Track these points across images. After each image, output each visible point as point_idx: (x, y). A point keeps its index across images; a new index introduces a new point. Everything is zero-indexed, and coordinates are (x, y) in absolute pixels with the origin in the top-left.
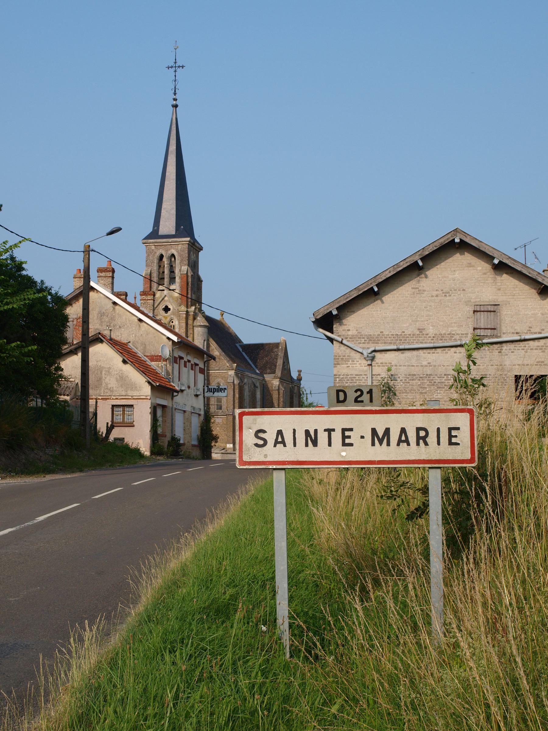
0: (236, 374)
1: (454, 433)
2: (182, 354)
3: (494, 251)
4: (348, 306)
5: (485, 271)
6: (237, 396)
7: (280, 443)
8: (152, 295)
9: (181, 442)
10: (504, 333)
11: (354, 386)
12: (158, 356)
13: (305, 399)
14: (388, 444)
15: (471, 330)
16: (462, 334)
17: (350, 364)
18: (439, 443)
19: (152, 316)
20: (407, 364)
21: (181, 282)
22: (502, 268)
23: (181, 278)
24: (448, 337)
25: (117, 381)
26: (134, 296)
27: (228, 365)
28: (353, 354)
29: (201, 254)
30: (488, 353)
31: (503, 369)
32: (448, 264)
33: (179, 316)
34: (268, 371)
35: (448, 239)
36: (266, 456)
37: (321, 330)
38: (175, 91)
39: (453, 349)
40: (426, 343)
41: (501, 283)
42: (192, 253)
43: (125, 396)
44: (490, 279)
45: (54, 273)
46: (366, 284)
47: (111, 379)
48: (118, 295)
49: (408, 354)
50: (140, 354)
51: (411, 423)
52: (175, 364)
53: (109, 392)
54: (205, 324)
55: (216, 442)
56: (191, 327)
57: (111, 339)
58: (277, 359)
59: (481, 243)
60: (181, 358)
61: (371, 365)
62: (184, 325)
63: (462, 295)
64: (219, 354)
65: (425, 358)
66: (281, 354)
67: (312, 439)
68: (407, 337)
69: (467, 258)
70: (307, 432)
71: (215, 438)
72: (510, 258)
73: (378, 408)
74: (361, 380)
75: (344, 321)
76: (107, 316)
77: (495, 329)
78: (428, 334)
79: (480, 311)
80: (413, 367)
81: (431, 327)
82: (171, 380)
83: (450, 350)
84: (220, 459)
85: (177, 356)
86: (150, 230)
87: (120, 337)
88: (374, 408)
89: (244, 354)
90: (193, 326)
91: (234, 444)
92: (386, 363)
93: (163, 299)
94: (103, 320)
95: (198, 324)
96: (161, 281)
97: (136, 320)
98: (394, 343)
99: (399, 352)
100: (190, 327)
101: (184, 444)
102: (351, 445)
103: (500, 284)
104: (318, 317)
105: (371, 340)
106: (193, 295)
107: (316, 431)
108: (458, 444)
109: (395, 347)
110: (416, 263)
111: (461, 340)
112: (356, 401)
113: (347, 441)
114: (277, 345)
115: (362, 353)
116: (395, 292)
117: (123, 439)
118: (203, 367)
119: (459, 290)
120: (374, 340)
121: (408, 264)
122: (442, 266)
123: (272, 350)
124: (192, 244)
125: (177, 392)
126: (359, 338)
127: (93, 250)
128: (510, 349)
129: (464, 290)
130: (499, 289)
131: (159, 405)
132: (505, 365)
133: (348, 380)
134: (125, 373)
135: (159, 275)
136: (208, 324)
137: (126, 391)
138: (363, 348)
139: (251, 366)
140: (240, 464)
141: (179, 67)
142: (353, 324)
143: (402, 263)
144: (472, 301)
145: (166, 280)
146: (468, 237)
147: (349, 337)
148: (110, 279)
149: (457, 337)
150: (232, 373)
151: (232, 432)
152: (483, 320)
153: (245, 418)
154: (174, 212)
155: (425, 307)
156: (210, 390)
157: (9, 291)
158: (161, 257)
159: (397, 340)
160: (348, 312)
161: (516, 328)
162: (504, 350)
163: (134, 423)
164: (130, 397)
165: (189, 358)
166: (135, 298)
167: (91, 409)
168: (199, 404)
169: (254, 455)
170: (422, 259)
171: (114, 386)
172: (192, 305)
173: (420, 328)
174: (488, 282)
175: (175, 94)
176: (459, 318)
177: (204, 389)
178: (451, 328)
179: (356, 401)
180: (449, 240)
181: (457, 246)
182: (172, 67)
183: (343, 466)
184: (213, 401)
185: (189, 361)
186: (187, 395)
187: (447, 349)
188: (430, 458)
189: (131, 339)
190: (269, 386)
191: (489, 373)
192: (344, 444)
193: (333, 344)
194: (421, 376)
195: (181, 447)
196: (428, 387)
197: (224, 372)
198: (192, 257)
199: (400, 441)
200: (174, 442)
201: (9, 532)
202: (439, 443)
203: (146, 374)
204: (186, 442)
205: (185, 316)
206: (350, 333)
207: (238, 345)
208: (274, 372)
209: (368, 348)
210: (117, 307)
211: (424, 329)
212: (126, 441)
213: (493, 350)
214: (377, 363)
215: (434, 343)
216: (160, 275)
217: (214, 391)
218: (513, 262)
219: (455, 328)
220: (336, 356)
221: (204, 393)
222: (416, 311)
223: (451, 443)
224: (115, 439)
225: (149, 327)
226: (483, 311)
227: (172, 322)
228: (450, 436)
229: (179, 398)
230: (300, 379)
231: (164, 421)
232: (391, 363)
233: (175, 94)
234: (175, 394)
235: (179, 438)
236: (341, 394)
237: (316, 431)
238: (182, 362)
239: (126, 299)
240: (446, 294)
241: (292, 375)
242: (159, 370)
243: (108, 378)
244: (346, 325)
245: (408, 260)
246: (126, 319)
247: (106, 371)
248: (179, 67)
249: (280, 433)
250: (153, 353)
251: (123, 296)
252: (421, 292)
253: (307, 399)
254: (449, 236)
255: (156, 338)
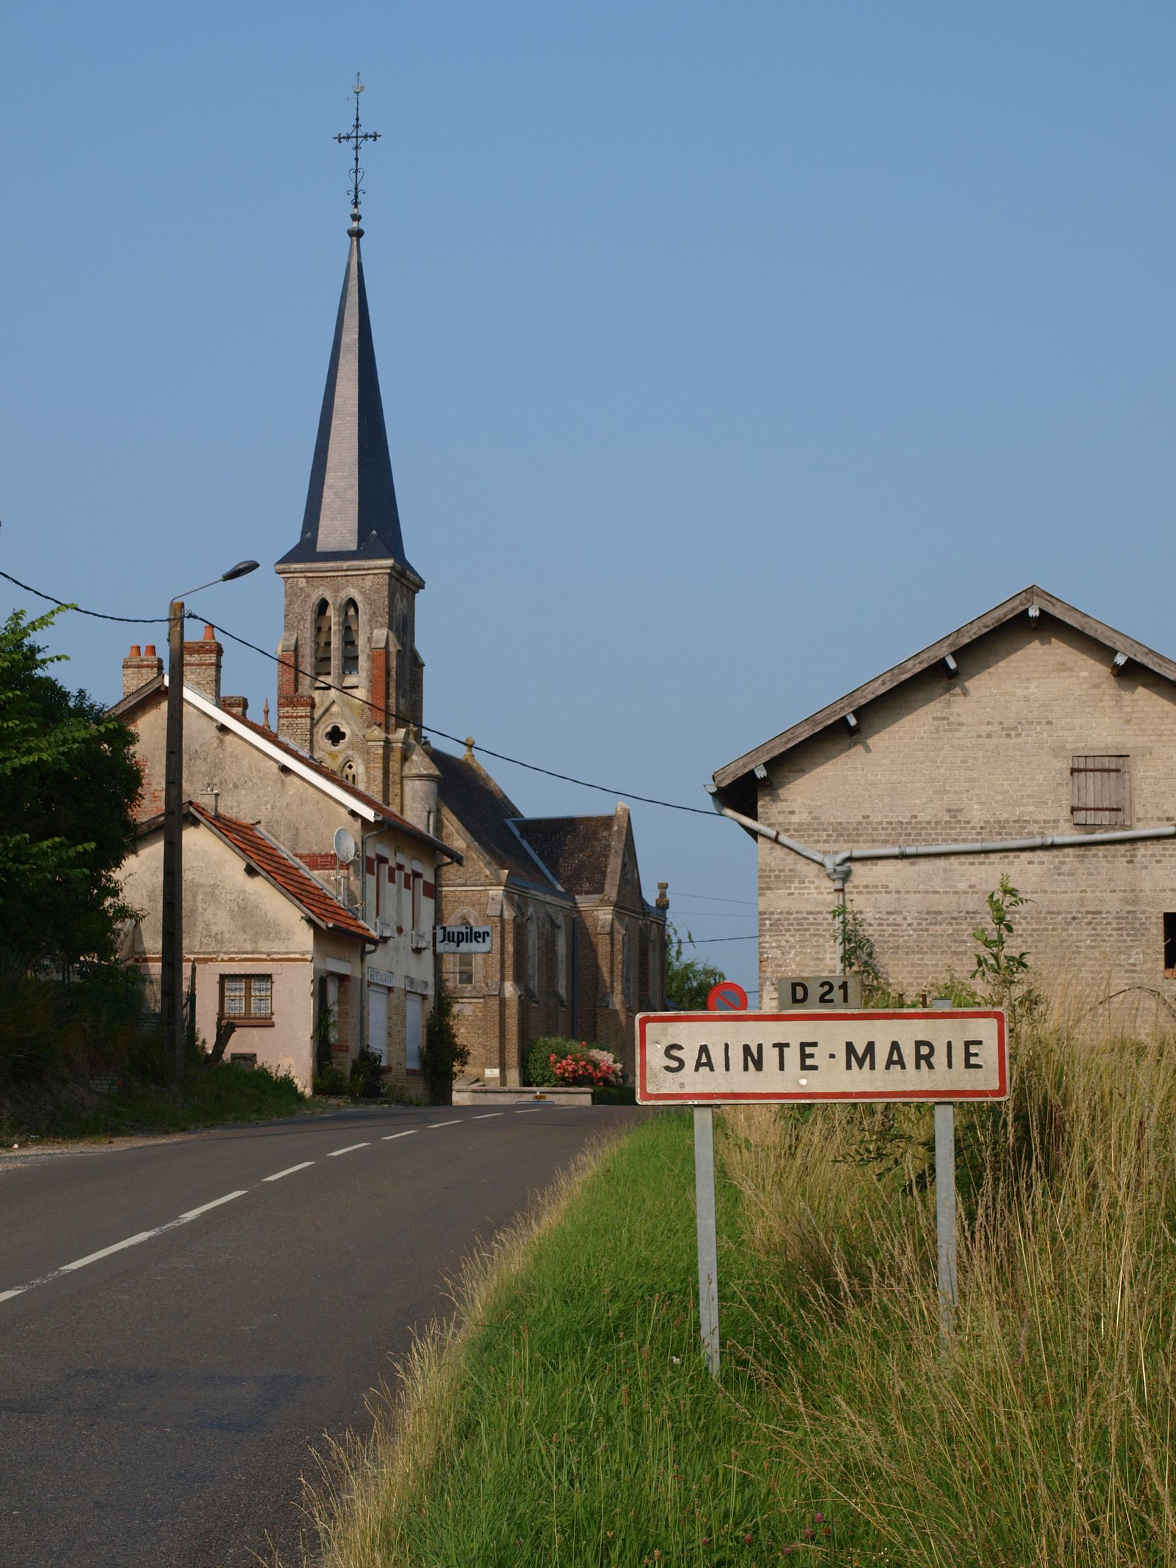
0: (508, 895)
1: (973, 1049)
2: (385, 852)
3: (1117, 636)
4: (792, 758)
5: (1096, 681)
6: (510, 948)
7: (704, 1065)
8: (307, 705)
9: (384, 1063)
10: (1139, 820)
11: (819, 977)
12: (327, 855)
13: (673, 953)
14: (872, 1067)
15: (1066, 813)
16: (1046, 822)
17: (796, 888)
18: (950, 1065)
19: (307, 756)
20: (922, 888)
21: (372, 669)
22: (1133, 673)
23: (372, 659)
24: (1014, 828)
25: (233, 917)
26: (263, 707)
27: (488, 872)
28: (802, 866)
29: (420, 597)
30: (1104, 864)
31: (1136, 902)
32: (1013, 665)
33: (367, 755)
34: (586, 886)
35: (1013, 610)
36: (682, 1085)
37: (729, 812)
38: (356, 197)
39: (1026, 855)
40: (964, 841)
41: (1133, 707)
42: (398, 596)
43: (252, 953)
44: (1107, 698)
45: (91, 668)
46: (830, 710)
47: (219, 912)
48: (224, 704)
49: (924, 865)
50: (285, 852)
51: (908, 1033)
52: (368, 876)
53: (213, 944)
54: (431, 772)
55: (464, 1063)
56: (397, 779)
57: (218, 817)
58: (607, 857)
59: (1087, 620)
60: (382, 860)
61: (842, 890)
62: (379, 774)
63: (1045, 734)
64: (464, 845)
65: (963, 875)
66: (617, 845)
67: (753, 1058)
68: (923, 828)
69: (1059, 650)
70: (747, 1049)
71: (462, 1055)
72: (1151, 651)
73: (856, 1011)
74: (821, 924)
75: (783, 792)
76: (205, 759)
77: (1118, 810)
78: (968, 822)
79: (1086, 770)
80: (936, 896)
81: (976, 807)
82: (360, 915)
83: (1018, 857)
84: (469, 1103)
85: (373, 857)
86: (293, 539)
87: (235, 810)
88: (849, 1012)
89: (524, 843)
90: (402, 778)
91: (503, 1067)
92: (876, 887)
93: (327, 710)
94: (195, 769)
95: (415, 771)
96: (322, 662)
97: (275, 769)
98: (894, 842)
99: (906, 862)
100: (395, 778)
101: (388, 1069)
102: (815, 1068)
103: (1129, 709)
104: (723, 784)
105: (842, 835)
106: (401, 700)
107: (760, 1047)
108: (980, 1067)
109: (895, 851)
110: (942, 663)
111: (1042, 834)
112: (822, 1000)
113: (809, 1062)
114: (607, 822)
115: (822, 865)
116: (895, 727)
117: (252, 1057)
118: (432, 881)
119: (1039, 723)
120: (849, 835)
121: (925, 665)
122: (1000, 670)
123: (595, 833)
124: (399, 573)
125: (375, 942)
126: (815, 830)
127: (191, 616)
128: (1152, 855)
129: (1049, 723)
130: (1128, 721)
131: (332, 974)
132: (1141, 891)
133: (792, 924)
134: (252, 898)
135: (317, 651)
136: (437, 773)
137: (256, 942)
138: (825, 853)
139: (542, 873)
140: (643, 1098)
141: (366, 137)
142: (803, 797)
143: (910, 664)
144: (1068, 746)
145: (335, 663)
146: (1059, 605)
147: (792, 827)
148: (212, 671)
149: (1036, 828)
150: (497, 892)
151: (497, 1040)
152: (1093, 790)
153: (649, 1026)
154: (353, 495)
155: (962, 762)
156: (448, 937)
157: (34, 725)
158: (323, 605)
159: (900, 834)
160: (790, 771)
161: (1165, 807)
162: (1139, 857)
163: (274, 1018)
164: (264, 956)
165: (401, 859)
166: (267, 712)
167: (185, 988)
168: (423, 970)
169: (668, 1084)
170: (955, 655)
171: (226, 929)
172: (398, 726)
173: (952, 807)
174: (1104, 704)
175: (356, 204)
176: (1039, 785)
177: (434, 935)
178: (1022, 809)
179: (822, 1000)
180: (1016, 612)
181: (1033, 625)
182: (348, 137)
183: (803, 1101)
184: (451, 965)
185: (400, 867)
186: (396, 949)
187: (1011, 854)
188: (936, 1089)
189: (264, 814)
190: (589, 923)
191: (1107, 908)
192: (804, 1067)
193: (756, 840)
194: (955, 914)
195: (382, 1077)
196: (969, 939)
197: (480, 890)
198: (399, 606)
199: (890, 1063)
200: (367, 1061)
201: (150, 1238)
202: (950, 1065)
203: (302, 901)
204: (394, 1063)
205: (381, 751)
206: (795, 819)
207: (509, 822)
208: (600, 890)
209: (836, 853)
210: (229, 738)
211: (961, 810)
212: (260, 1060)
213: (1114, 856)
214: (856, 887)
215: (983, 840)
216: (321, 649)
217: (459, 938)
218: (1156, 660)
219: (1031, 809)
220: (764, 871)
221: (434, 945)
222: (942, 770)
223: (968, 1065)
224: (235, 1057)
225: (307, 785)
226: (1093, 770)
227: (350, 767)
228: (968, 1055)
229: (377, 959)
230: (663, 906)
231: (343, 1014)
232: (887, 887)
233: (356, 204)
234: (369, 947)
235: (379, 1053)
236: (799, 990)
237: (760, 1047)
238: (385, 869)
239: (244, 714)
240: (1009, 731)
241: (644, 895)
242: (330, 891)
243: (211, 909)
244: (786, 800)
245: (924, 656)
246: (250, 767)
247: (206, 893)
248: (366, 137)
249: (704, 1049)
250: (316, 850)
251: (237, 706)
252: (954, 727)
253: (679, 953)
254: (1017, 602)
255: (324, 812)
